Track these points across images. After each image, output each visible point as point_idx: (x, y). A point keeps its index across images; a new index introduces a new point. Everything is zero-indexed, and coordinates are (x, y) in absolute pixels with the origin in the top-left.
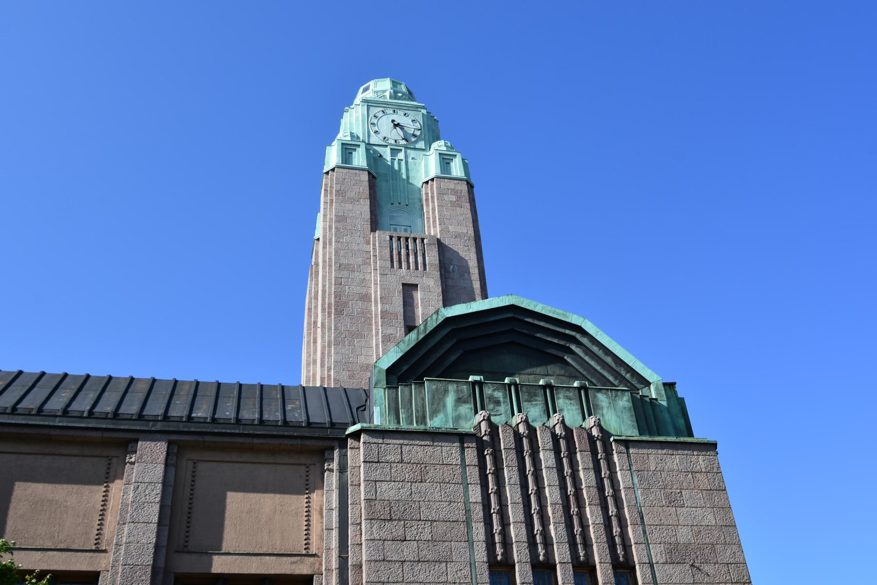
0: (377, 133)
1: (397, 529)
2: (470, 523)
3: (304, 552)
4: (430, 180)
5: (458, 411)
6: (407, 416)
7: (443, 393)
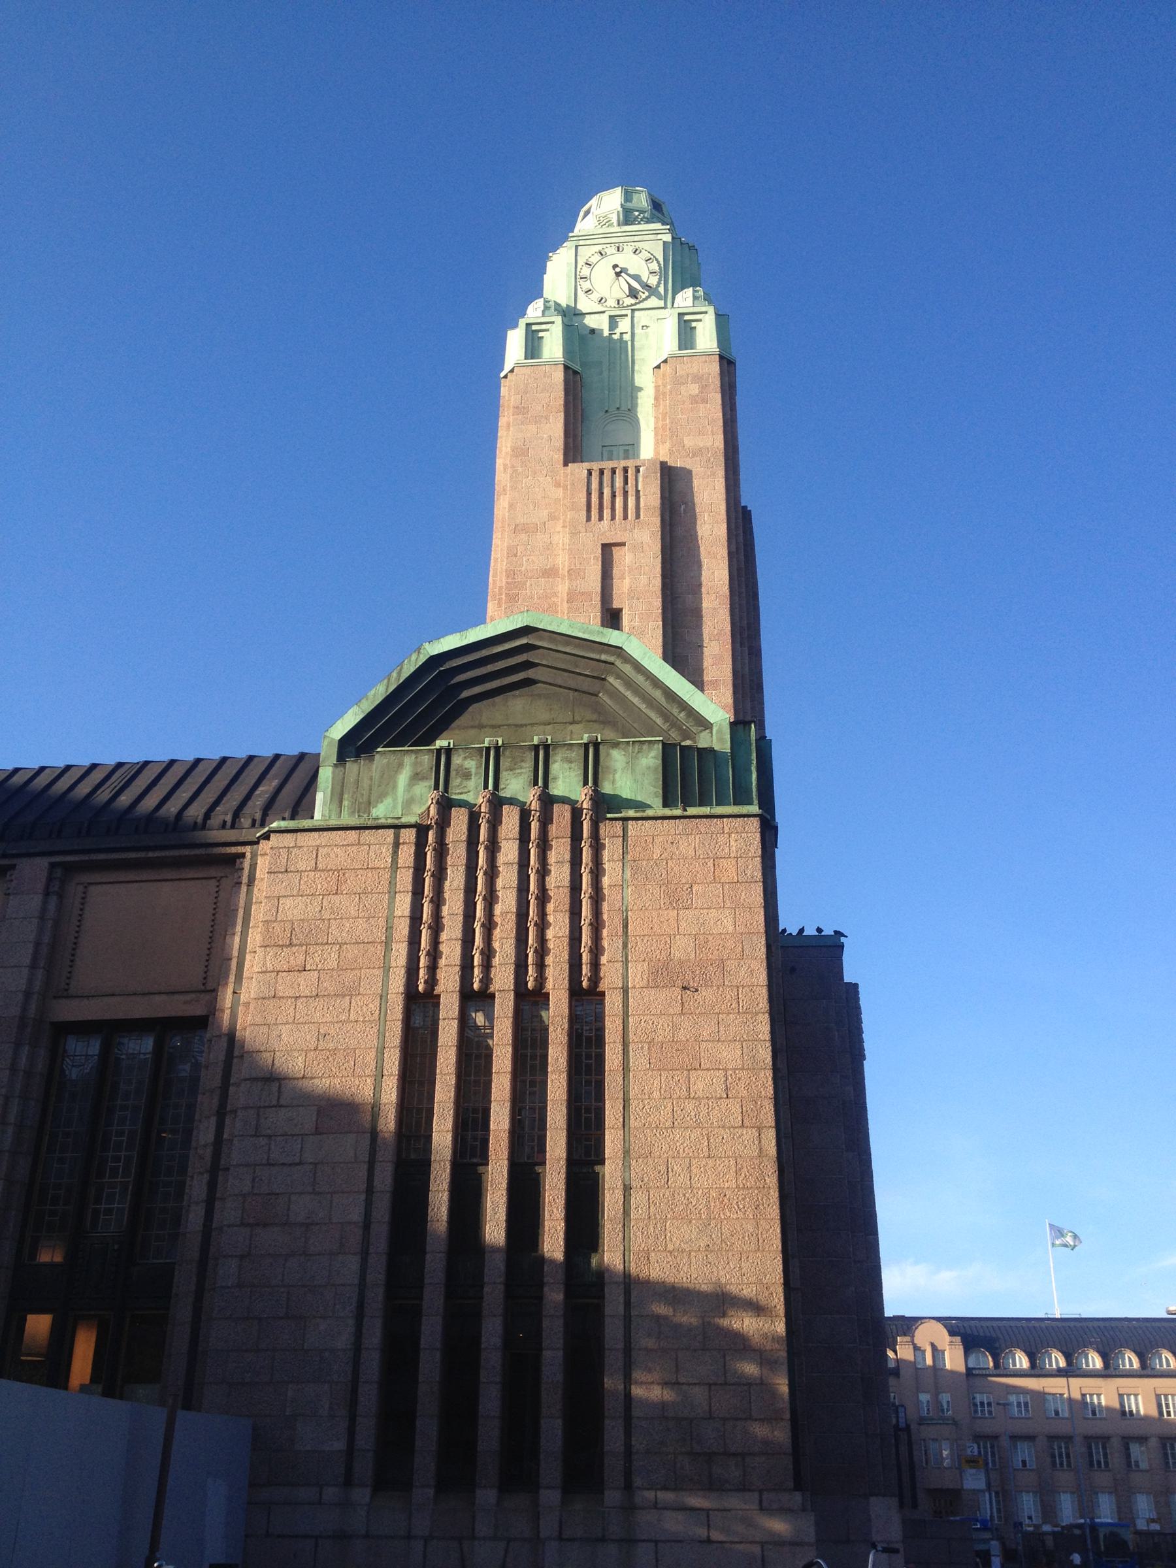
0: (590, 292)
1: (295, 957)
2: (390, 944)
3: (203, 988)
4: (662, 362)
7: (395, 769)
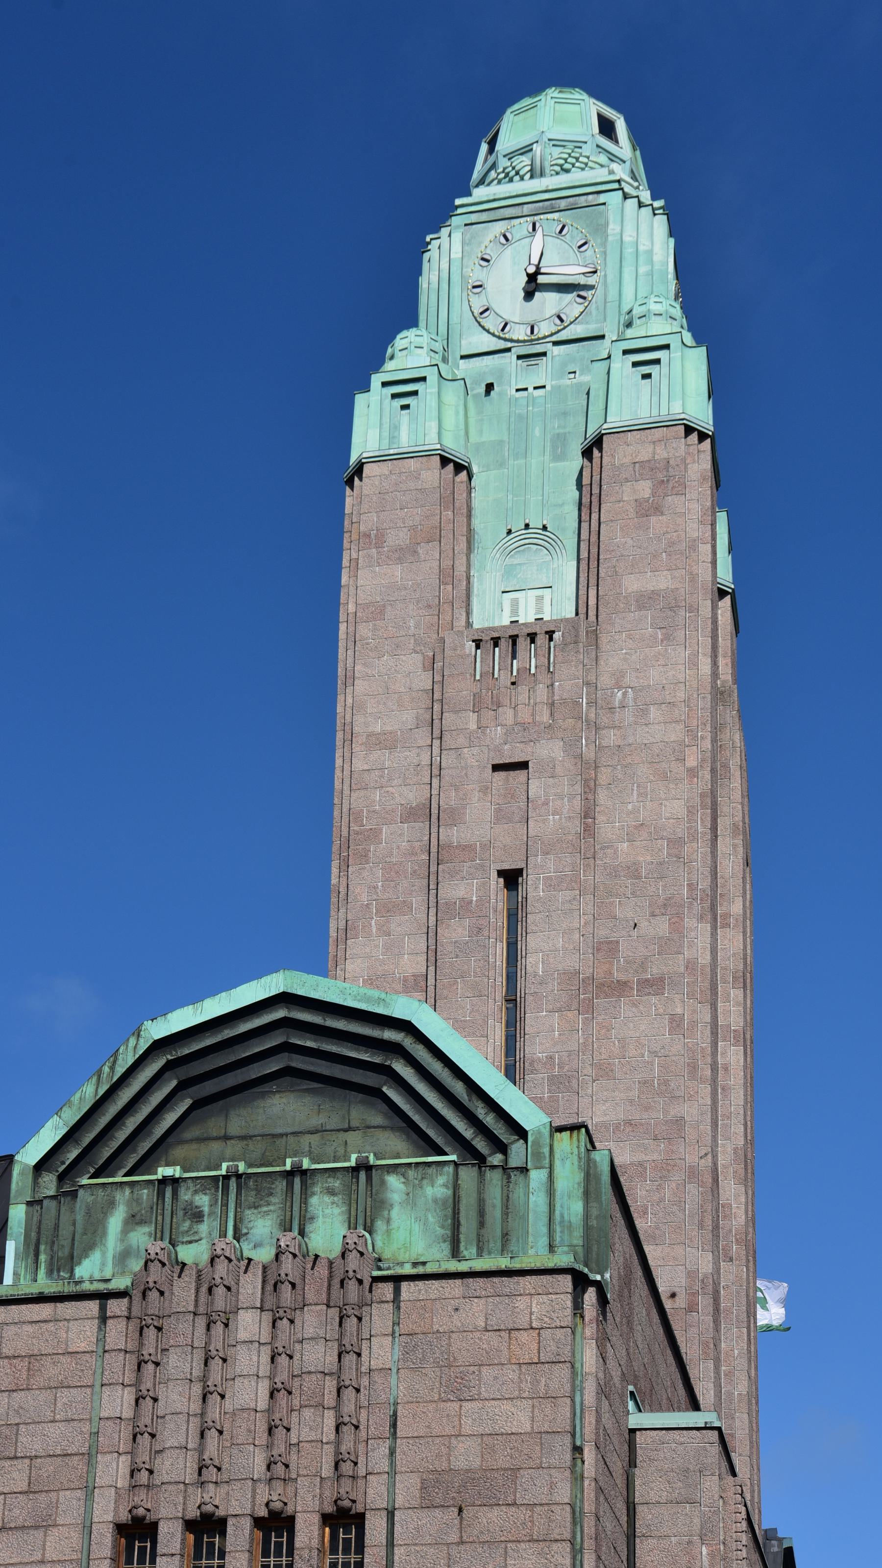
5: (126, 1241)
6: (50, 1257)
